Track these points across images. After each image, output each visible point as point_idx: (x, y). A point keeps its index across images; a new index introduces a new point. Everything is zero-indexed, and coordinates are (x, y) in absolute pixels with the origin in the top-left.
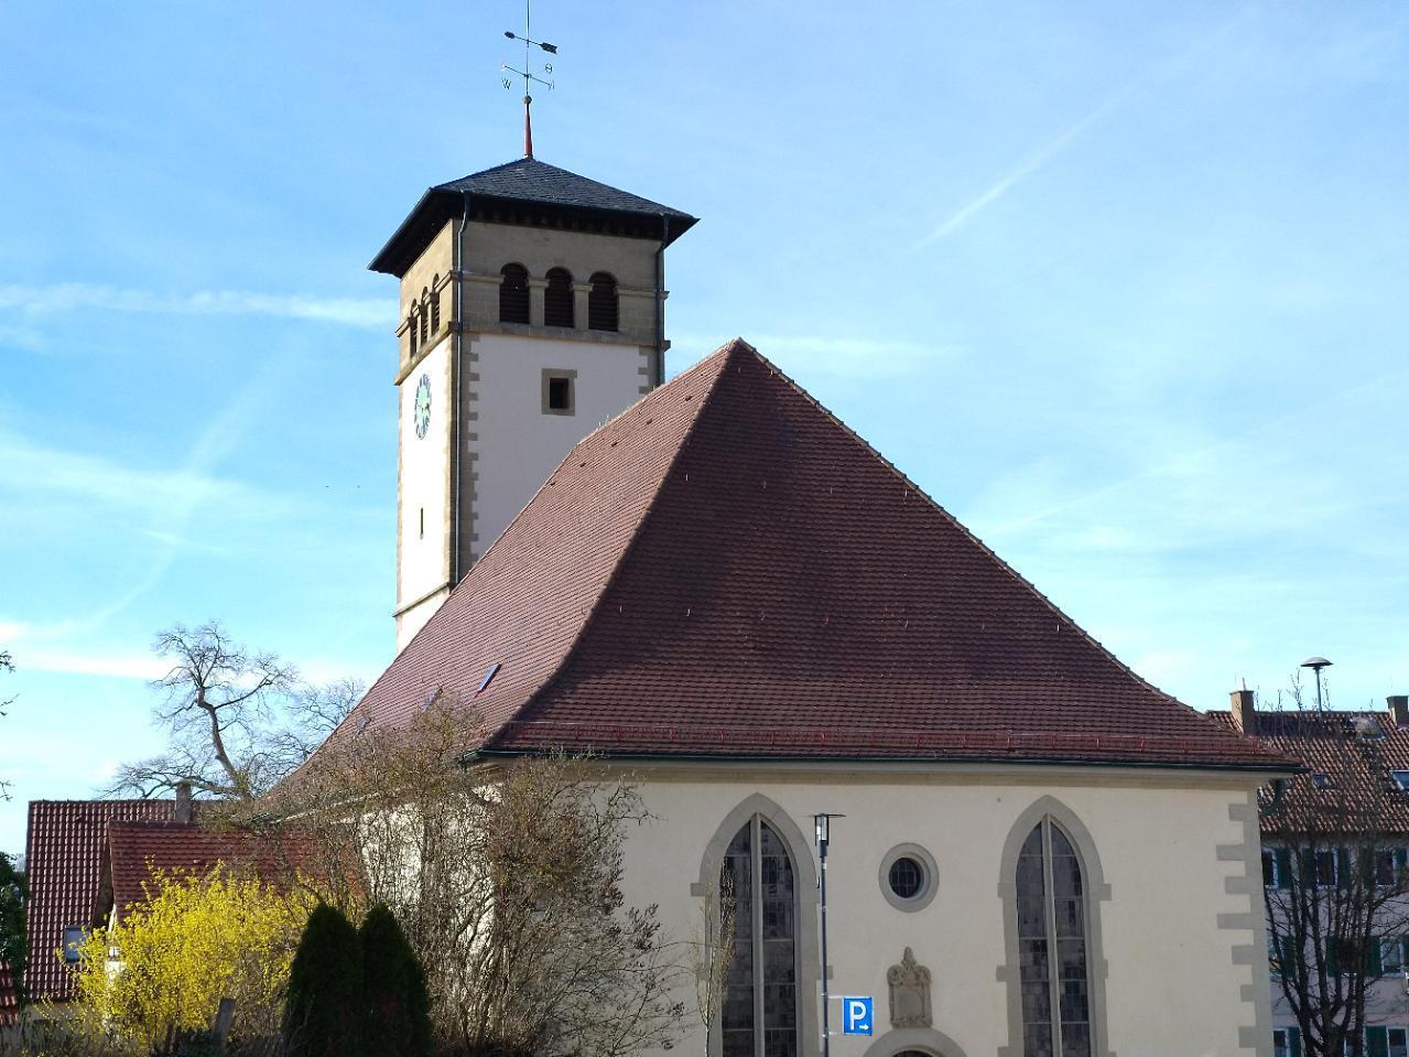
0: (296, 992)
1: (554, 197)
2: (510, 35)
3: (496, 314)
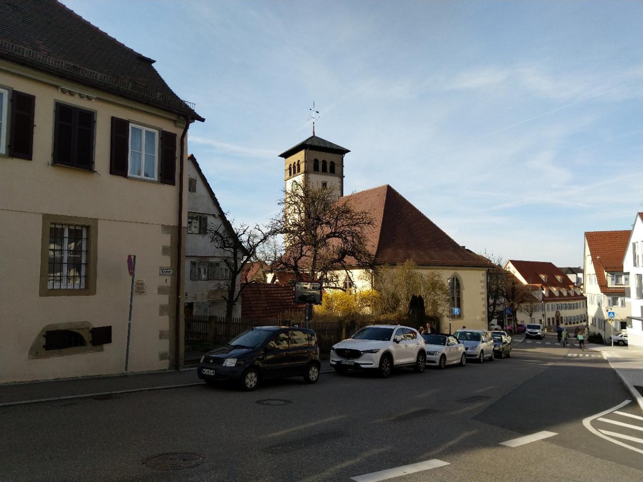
0: (405, 316)
1: (322, 145)
2: (318, 112)
3: (313, 169)
